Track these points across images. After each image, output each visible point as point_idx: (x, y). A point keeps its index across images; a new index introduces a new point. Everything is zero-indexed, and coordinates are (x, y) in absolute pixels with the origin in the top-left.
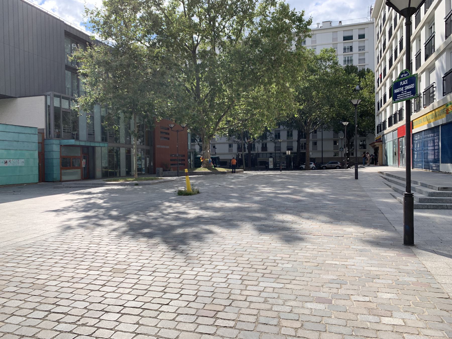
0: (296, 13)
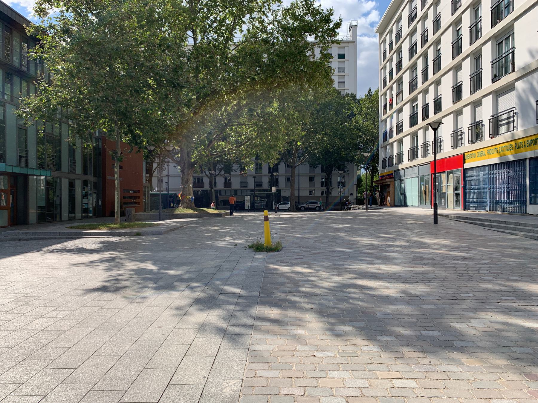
0: (323, 10)
